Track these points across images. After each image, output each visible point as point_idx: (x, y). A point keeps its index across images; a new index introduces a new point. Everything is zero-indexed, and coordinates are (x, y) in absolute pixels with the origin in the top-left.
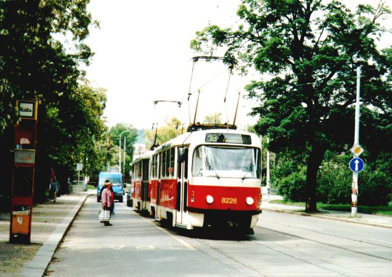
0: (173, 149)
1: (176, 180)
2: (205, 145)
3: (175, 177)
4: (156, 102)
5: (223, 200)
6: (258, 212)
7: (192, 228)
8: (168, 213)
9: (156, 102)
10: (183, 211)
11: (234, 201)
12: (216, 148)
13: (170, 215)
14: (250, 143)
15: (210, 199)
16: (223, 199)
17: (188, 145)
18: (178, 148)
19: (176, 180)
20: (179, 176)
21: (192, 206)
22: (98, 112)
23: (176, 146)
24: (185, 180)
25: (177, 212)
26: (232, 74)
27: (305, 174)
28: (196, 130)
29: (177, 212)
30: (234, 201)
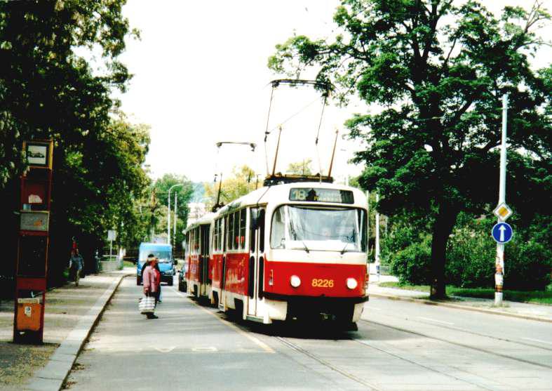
0: (244, 210)
1: (248, 254)
2: (289, 205)
3: (247, 250)
4: (220, 144)
5: (314, 282)
6: (364, 299)
7: (271, 322)
9: (220, 144)
11: (330, 283)
12: (304, 209)
13: (239, 303)
14: (353, 202)
15: (296, 281)
16: (313, 281)
17: (264, 205)
18: (251, 208)
20: (252, 248)
21: (270, 291)
22: (138, 158)
24: (260, 255)
25: (250, 300)
28: (276, 183)
29: (250, 300)
30: (330, 283)
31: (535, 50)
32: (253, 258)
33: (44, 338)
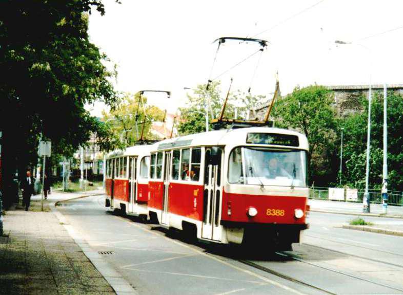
0: (125, 158)
1: (203, 187)
2: (245, 147)
3: (201, 182)
4: (223, 40)
5: (268, 212)
6: (305, 227)
7: (227, 243)
8: (151, 213)
9: (223, 40)
10: (214, 225)
11: (280, 213)
12: (257, 150)
13: (123, 206)
14: (298, 145)
15: (253, 212)
16: (267, 210)
17: (137, 156)
18: (166, 152)
19: (203, 187)
20: (206, 181)
21: (140, 200)
22: (87, 55)
23: (191, 147)
24: (135, 181)
25: (204, 225)
26: (195, 93)
27: (386, 187)
28: (142, 144)
29: (204, 225)
30: (280, 213)
31: (244, 93)
32: (207, 190)
33: (4, 228)
